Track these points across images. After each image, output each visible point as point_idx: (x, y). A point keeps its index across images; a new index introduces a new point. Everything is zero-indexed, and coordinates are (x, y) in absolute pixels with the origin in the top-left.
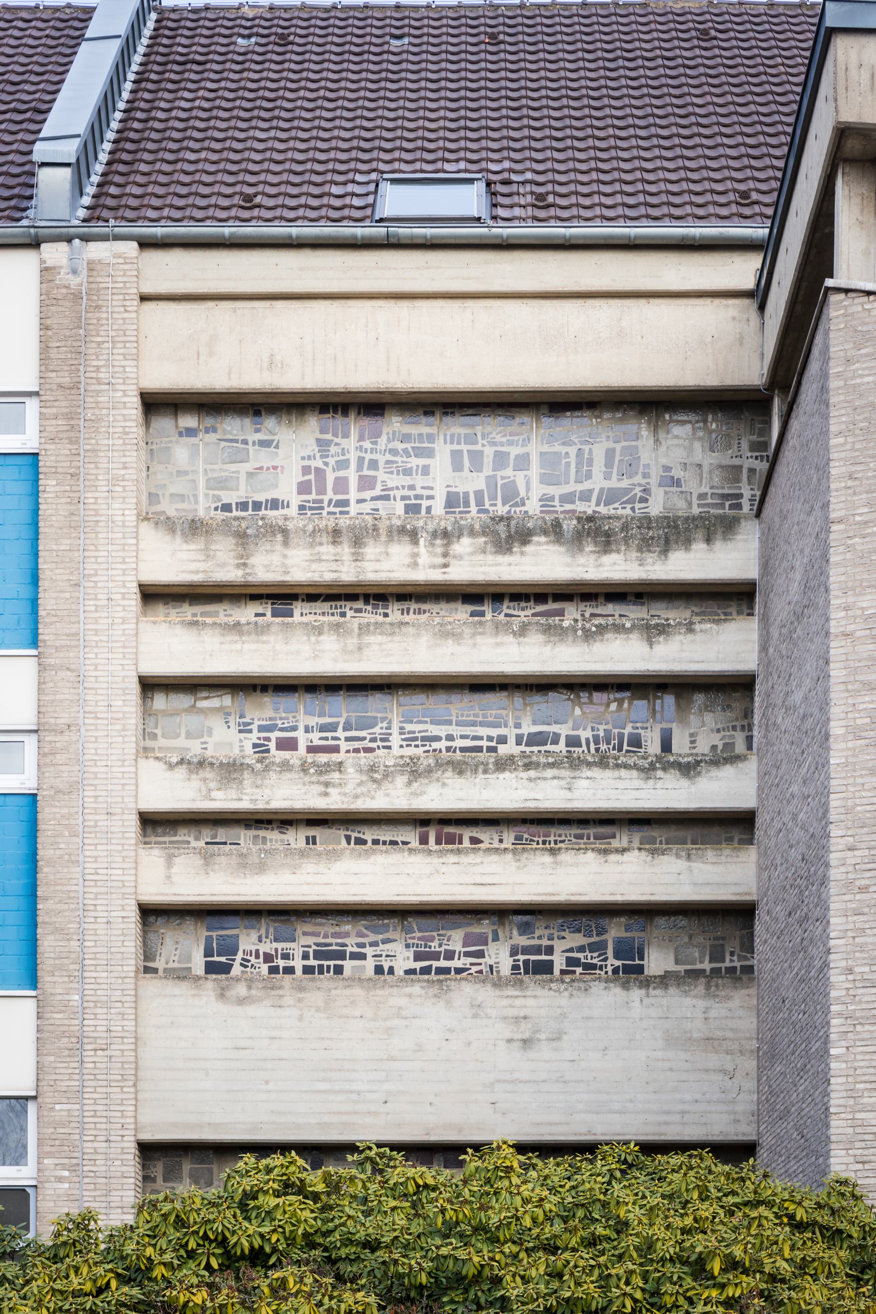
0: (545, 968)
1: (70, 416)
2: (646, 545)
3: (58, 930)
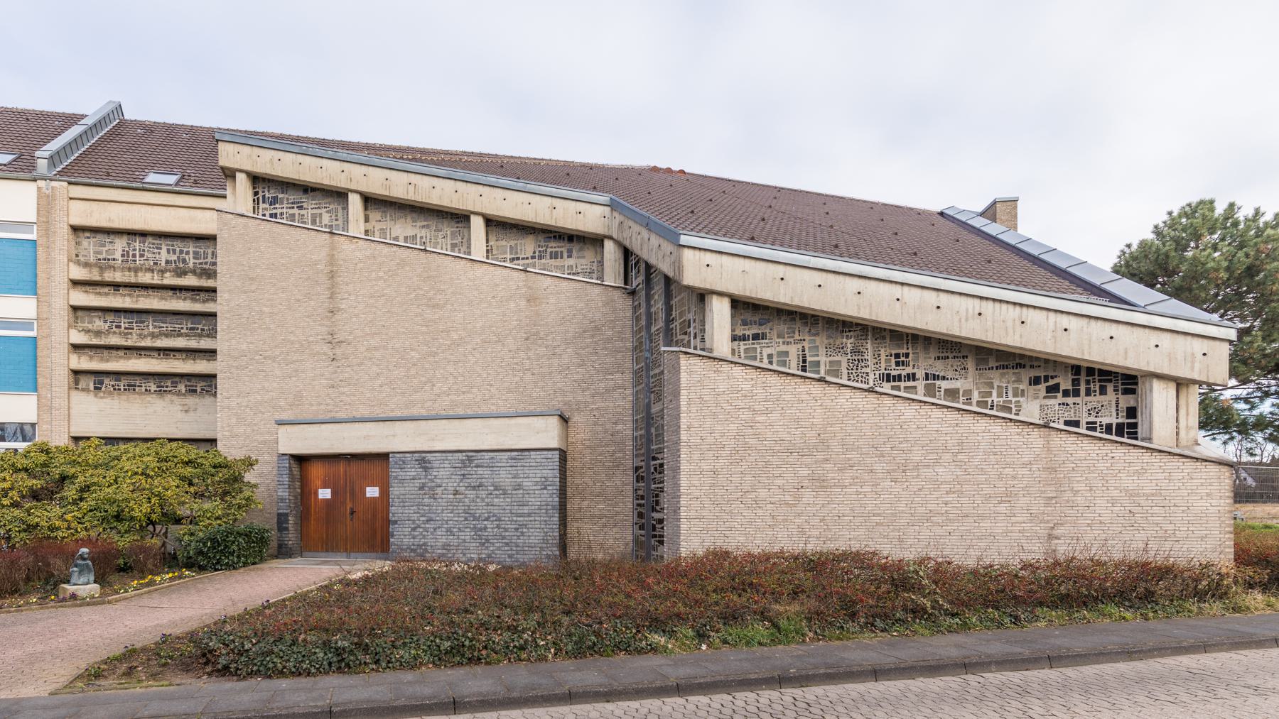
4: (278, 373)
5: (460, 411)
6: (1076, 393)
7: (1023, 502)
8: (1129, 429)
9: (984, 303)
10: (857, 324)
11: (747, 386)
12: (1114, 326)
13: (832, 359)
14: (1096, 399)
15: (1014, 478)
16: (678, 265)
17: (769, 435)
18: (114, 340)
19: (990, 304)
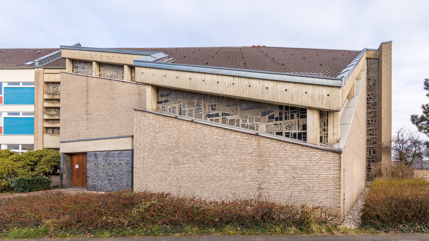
4: (74, 125)
6: (281, 119)
7: (249, 171)
9: (235, 78)
10: (198, 93)
12: (287, 84)
13: (190, 109)
14: (289, 121)
15: (245, 160)
17: (160, 142)
19: (237, 78)
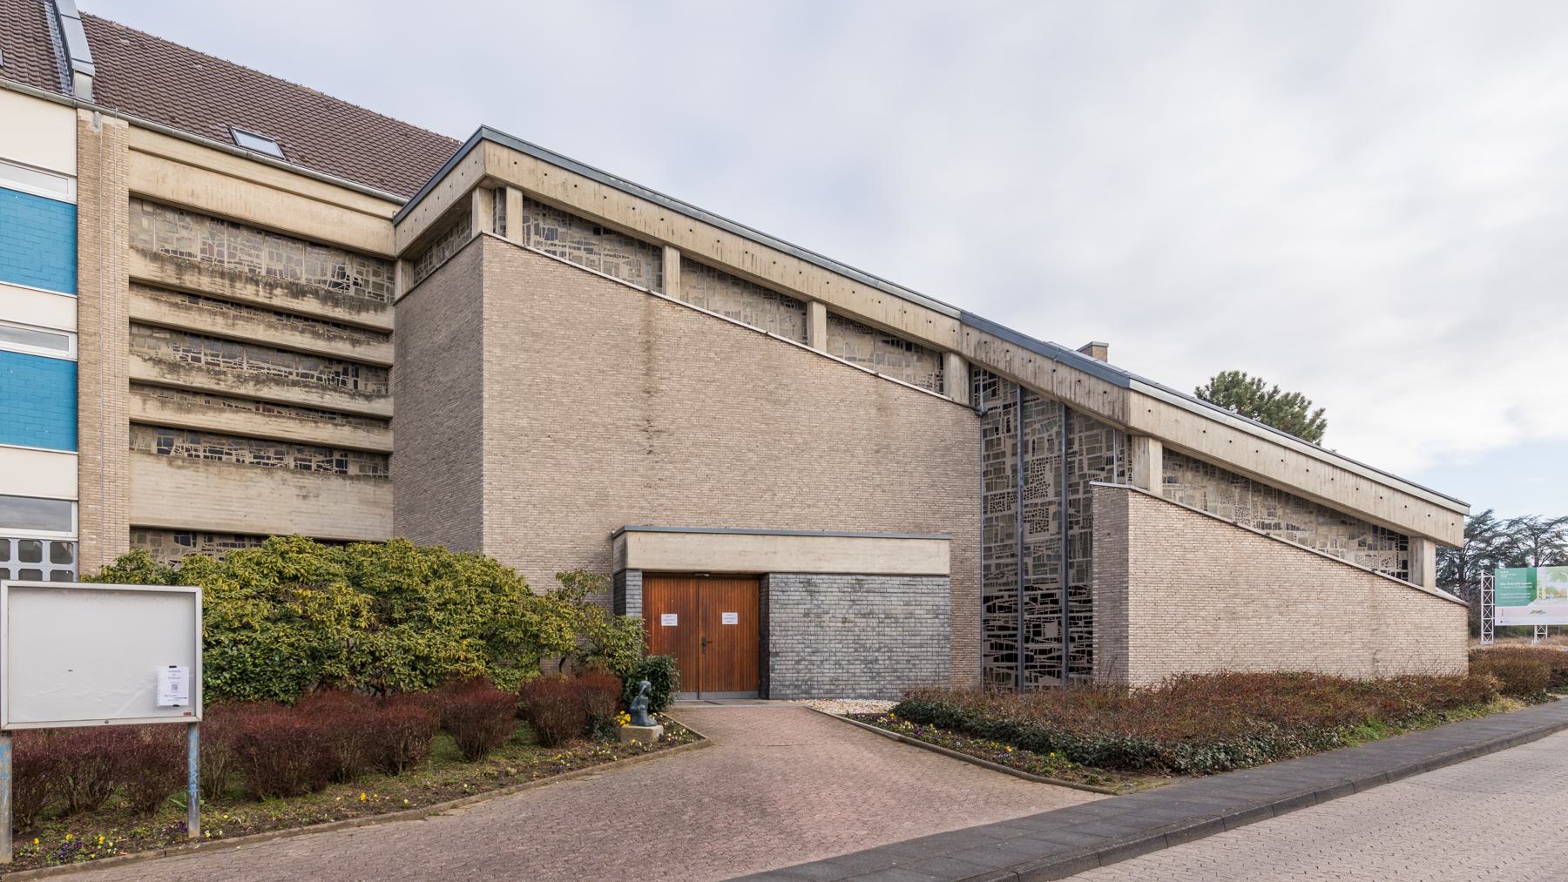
0: (308, 468)
1: (94, 192)
2: (351, 307)
3: (91, 426)
4: (575, 463)
5: (805, 527)
7: (1358, 633)
8: (1404, 573)
11: (1179, 525)
16: (1125, 408)
18: (200, 381)
